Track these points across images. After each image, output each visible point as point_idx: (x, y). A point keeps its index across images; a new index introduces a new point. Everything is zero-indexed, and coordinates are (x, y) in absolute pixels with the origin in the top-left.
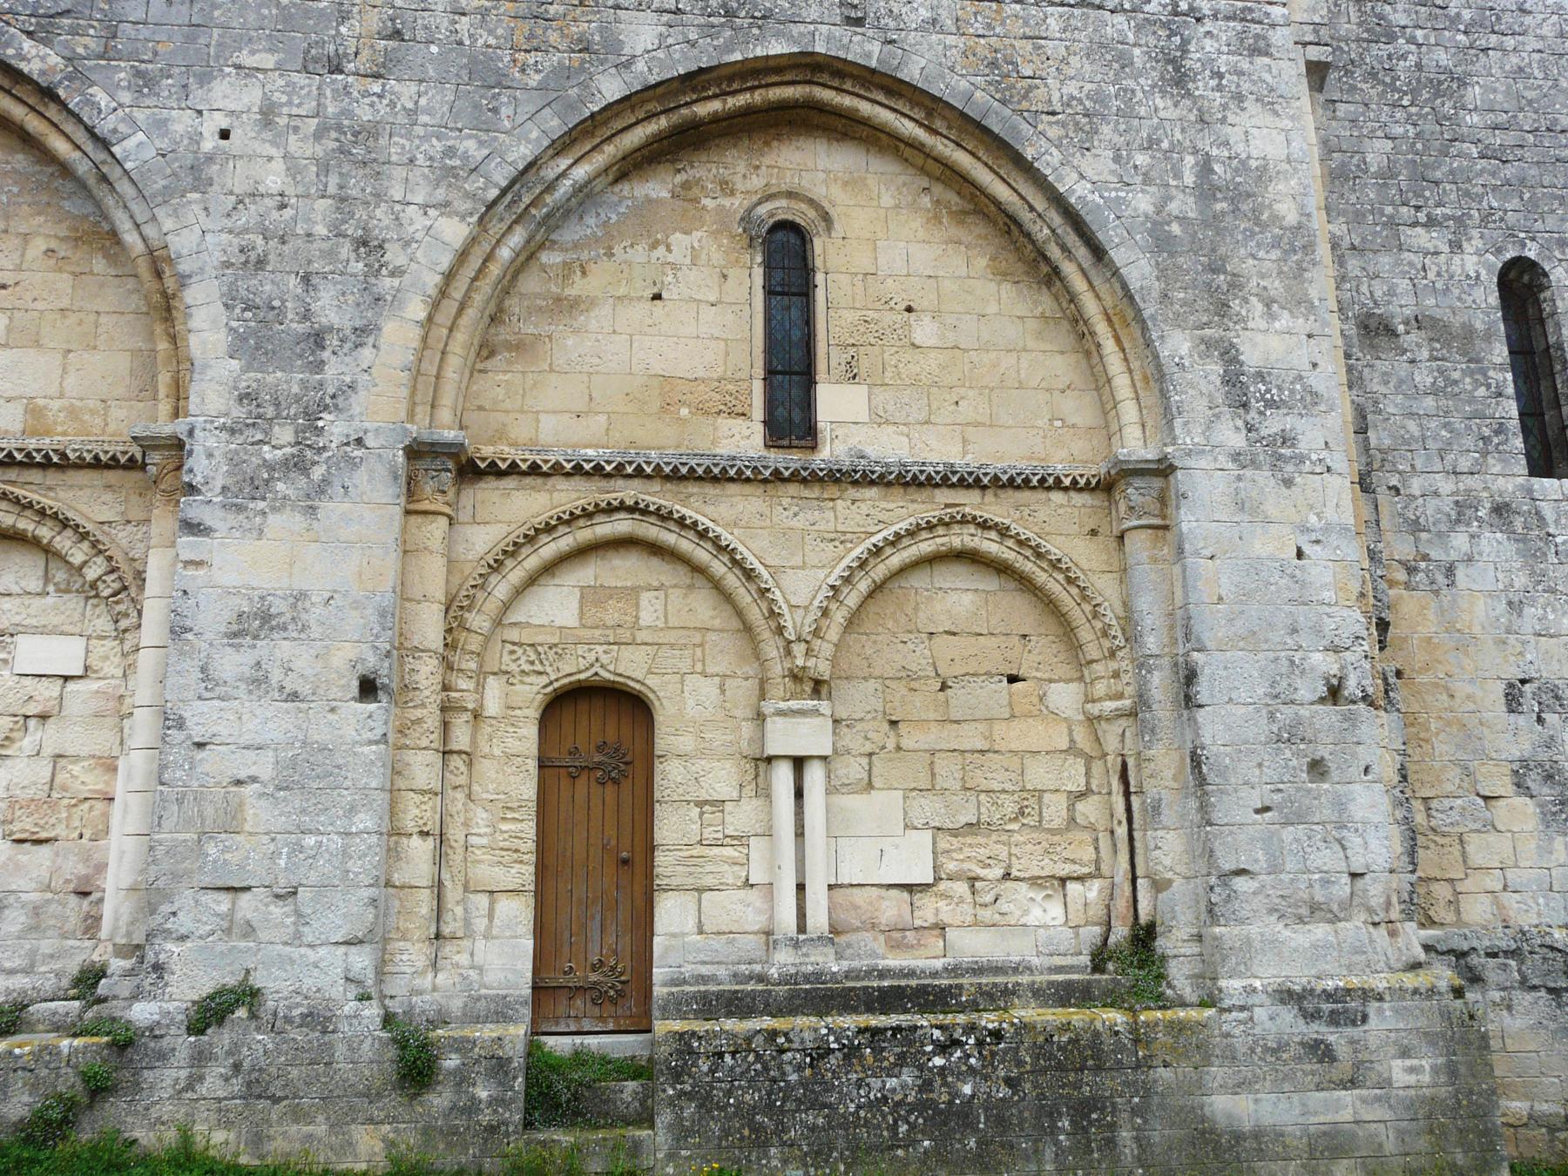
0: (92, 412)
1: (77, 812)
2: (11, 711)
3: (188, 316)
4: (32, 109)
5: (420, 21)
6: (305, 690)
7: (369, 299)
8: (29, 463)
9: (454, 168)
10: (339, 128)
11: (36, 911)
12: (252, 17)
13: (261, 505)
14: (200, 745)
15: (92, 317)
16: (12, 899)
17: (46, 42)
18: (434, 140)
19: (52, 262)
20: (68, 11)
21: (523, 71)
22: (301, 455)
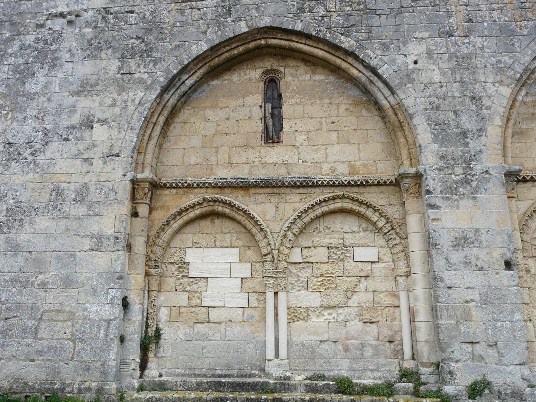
0: (372, 165)
1: (384, 311)
2: (356, 275)
3: (416, 129)
4: (343, 60)
5: (478, 15)
6: (486, 266)
7: (480, 119)
8: (356, 185)
9: (502, 67)
10: (456, 56)
11: (376, 348)
12: (417, 20)
13: (456, 197)
14: (450, 288)
15: (366, 131)
16: (366, 343)
17: (348, 36)
18: (492, 58)
19: (348, 113)
20: (354, 25)
21: (521, 29)
22: (466, 178)
